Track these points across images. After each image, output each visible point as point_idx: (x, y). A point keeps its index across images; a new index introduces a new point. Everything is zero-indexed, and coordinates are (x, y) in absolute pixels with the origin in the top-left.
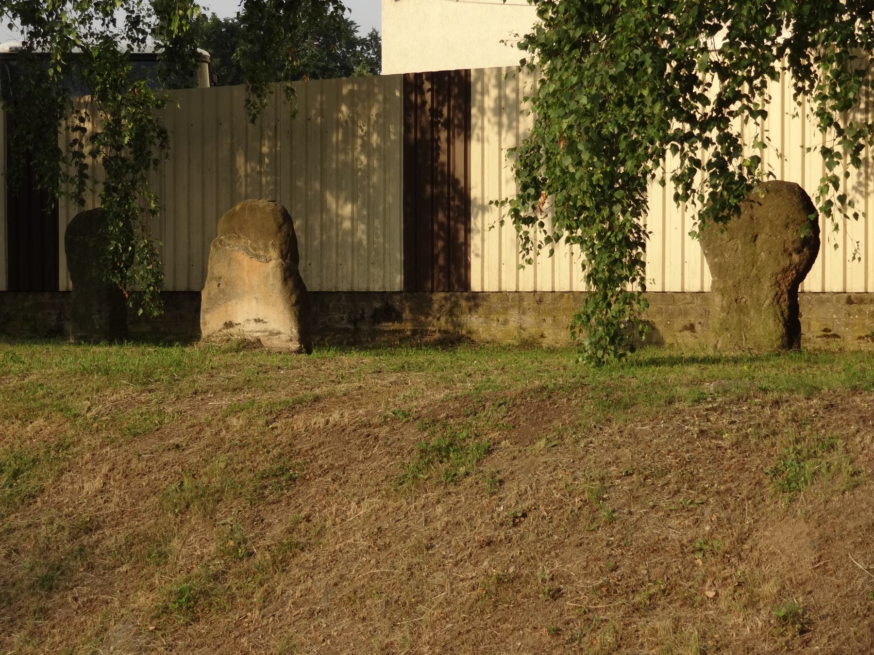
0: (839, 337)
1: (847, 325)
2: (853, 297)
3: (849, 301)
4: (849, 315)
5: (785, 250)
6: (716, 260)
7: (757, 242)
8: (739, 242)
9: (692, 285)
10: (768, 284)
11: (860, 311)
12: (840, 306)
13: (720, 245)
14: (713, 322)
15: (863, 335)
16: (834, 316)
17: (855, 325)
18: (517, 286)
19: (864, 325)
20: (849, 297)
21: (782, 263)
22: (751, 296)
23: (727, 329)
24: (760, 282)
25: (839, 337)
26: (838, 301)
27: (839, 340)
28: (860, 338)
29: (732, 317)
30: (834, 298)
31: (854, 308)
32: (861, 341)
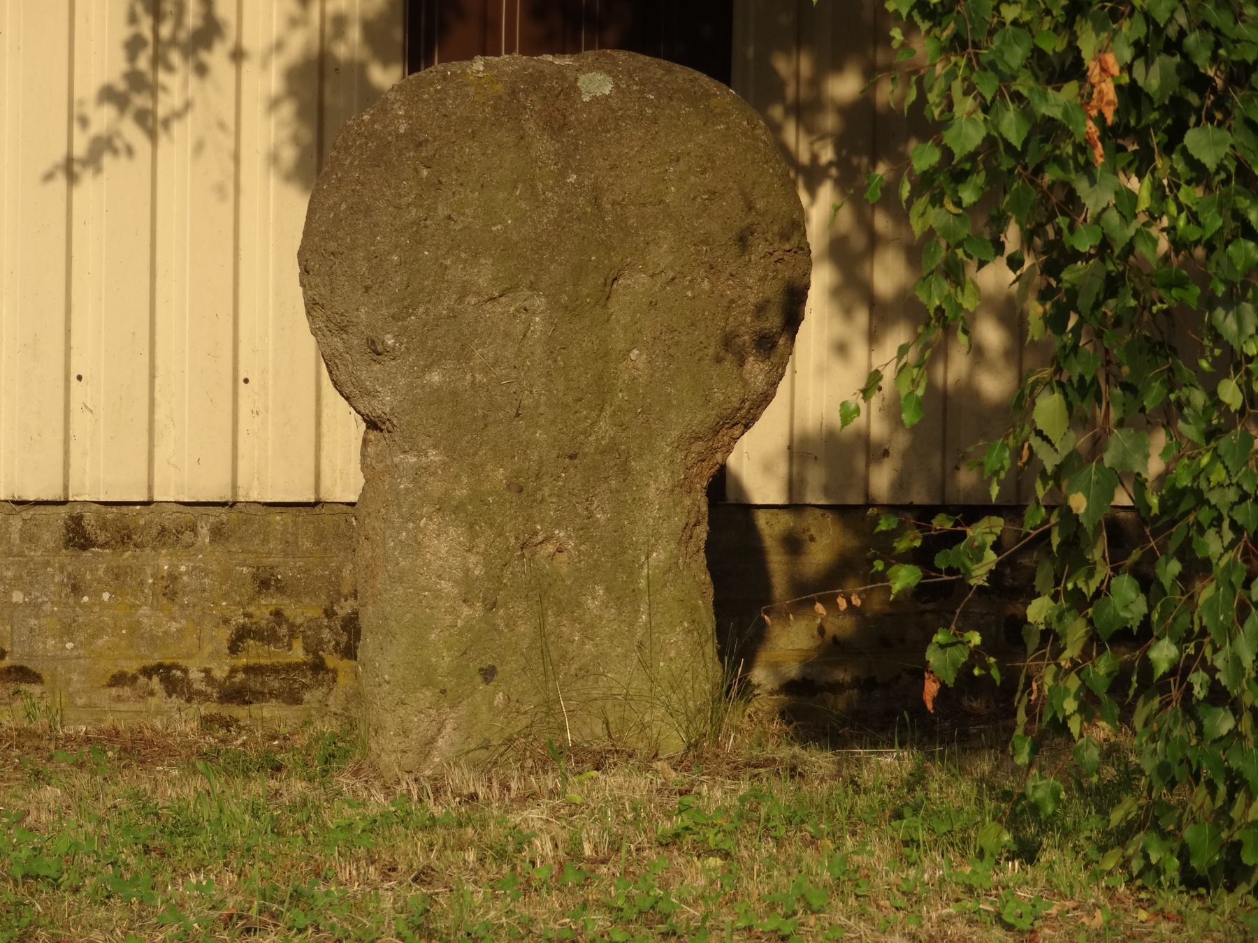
0: (35, 678)
1: (67, 631)
2: (89, 518)
3: (77, 536)
4: (76, 589)
5: (728, 341)
6: (435, 377)
7: (613, 306)
8: (539, 302)
9: (275, 476)
10: (665, 478)
11: (118, 575)
12: (37, 554)
13: (454, 315)
14: (646, 651)
15: (131, 667)
16: (17, 597)
17: (99, 631)
18: (66, 488)
19: (135, 628)
20: (77, 520)
21: (718, 396)
22: (585, 531)
23: (488, 674)
24: (624, 470)
25: (35, 678)
26: (29, 538)
27: (36, 689)
28: (119, 680)
29: (511, 623)
30: (16, 523)
31: (97, 563)
32: (126, 691)
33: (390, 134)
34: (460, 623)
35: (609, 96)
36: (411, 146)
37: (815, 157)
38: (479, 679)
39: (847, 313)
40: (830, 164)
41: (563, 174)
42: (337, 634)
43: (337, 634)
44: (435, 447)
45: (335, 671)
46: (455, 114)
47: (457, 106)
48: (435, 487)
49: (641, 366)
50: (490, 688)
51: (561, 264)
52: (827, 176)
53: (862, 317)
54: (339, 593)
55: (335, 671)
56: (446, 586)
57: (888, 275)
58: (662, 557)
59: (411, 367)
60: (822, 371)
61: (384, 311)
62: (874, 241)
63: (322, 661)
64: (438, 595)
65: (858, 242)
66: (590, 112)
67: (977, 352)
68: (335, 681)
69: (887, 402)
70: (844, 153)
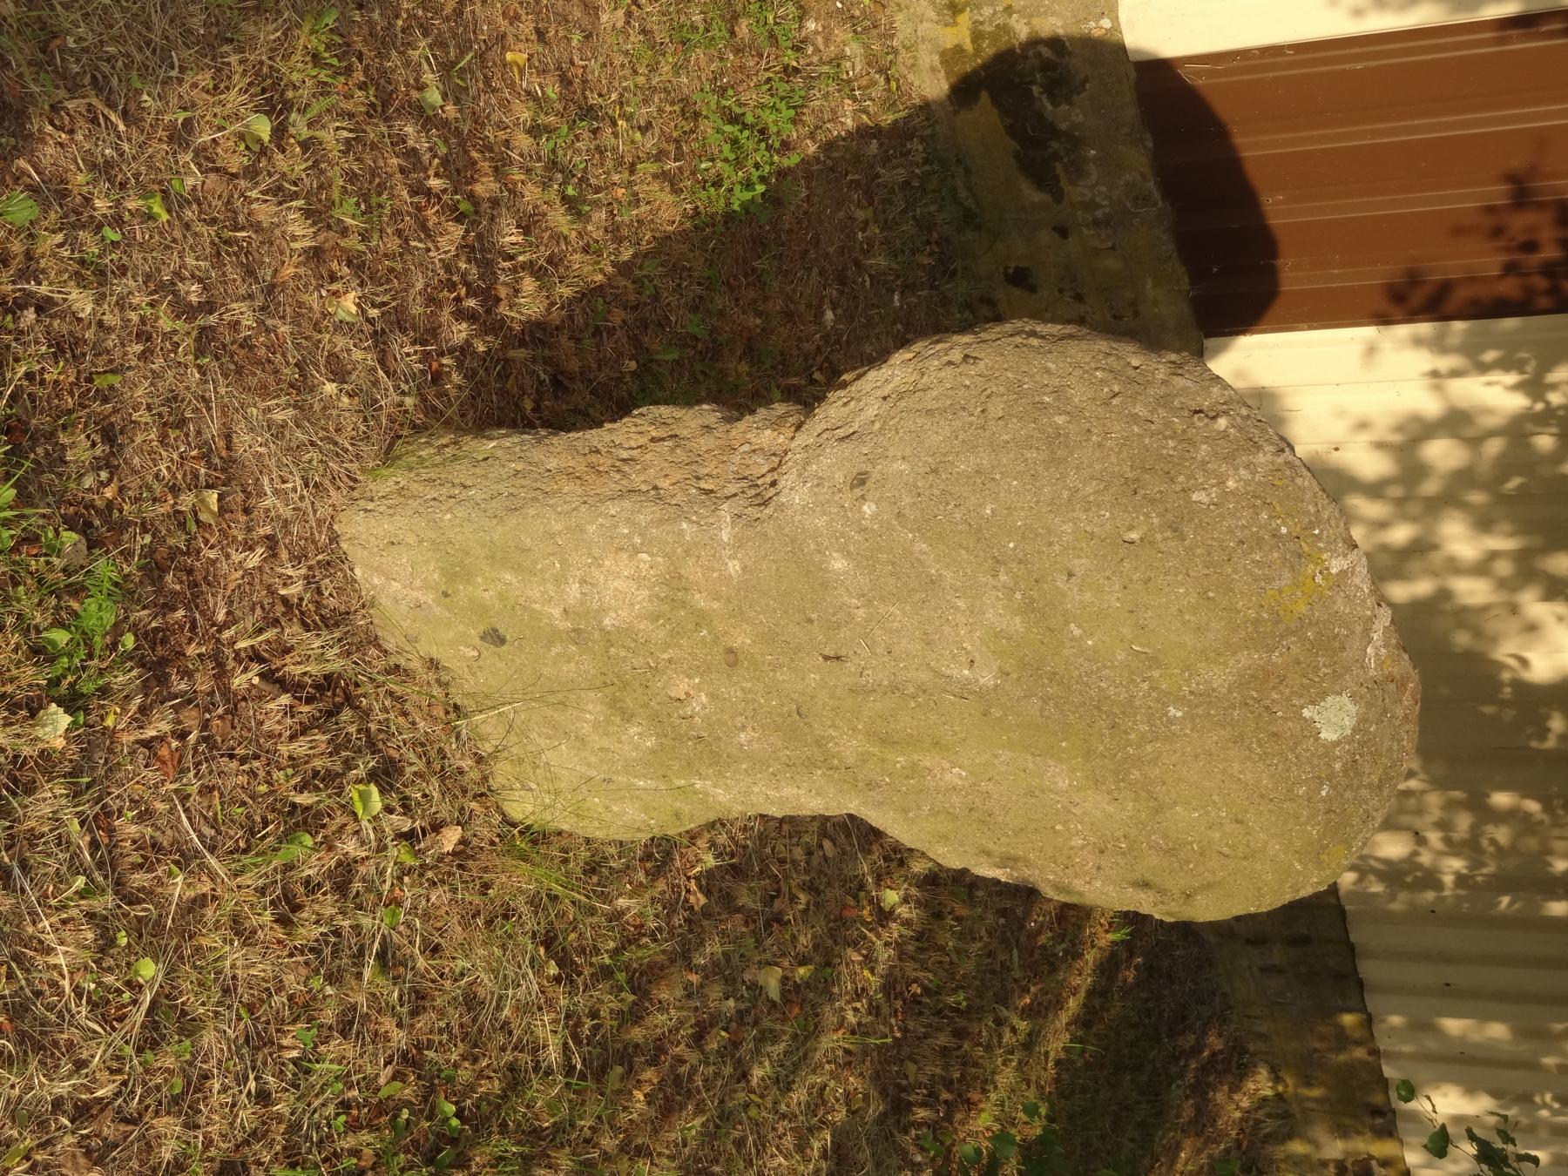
6: (838, 564)
33: (1188, 478)
34: (537, 606)
35: (1318, 739)
36: (1170, 516)
37: (1554, 387)
38: (481, 628)
39: (1399, 428)
40: (1548, 403)
41: (1179, 701)
42: (991, 22)
43: (991, 22)
44: (744, 569)
45: (955, 24)
46: (1235, 571)
47: (1249, 572)
48: (692, 571)
49: (948, 777)
50: (478, 641)
51: (1041, 710)
52: (1535, 401)
53: (1397, 438)
54: (1031, 16)
55: (955, 24)
56: (574, 590)
57: (1442, 454)
58: (721, 798)
59: (843, 535)
60: (1340, 413)
61: (907, 500)
62: (1475, 442)
63: (962, 11)
64: (561, 580)
65: (1470, 432)
66: (1286, 719)
67: (1382, 525)
68: (946, 25)
69: (1325, 457)
70: (1561, 413)
